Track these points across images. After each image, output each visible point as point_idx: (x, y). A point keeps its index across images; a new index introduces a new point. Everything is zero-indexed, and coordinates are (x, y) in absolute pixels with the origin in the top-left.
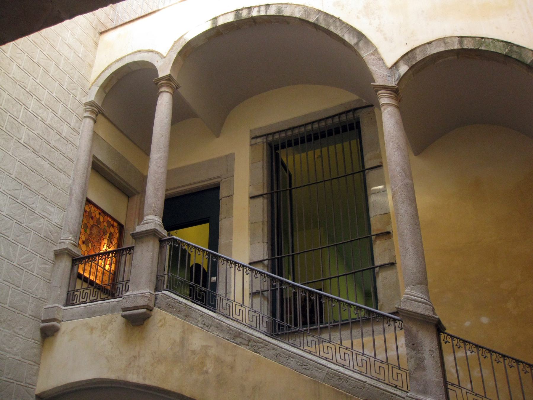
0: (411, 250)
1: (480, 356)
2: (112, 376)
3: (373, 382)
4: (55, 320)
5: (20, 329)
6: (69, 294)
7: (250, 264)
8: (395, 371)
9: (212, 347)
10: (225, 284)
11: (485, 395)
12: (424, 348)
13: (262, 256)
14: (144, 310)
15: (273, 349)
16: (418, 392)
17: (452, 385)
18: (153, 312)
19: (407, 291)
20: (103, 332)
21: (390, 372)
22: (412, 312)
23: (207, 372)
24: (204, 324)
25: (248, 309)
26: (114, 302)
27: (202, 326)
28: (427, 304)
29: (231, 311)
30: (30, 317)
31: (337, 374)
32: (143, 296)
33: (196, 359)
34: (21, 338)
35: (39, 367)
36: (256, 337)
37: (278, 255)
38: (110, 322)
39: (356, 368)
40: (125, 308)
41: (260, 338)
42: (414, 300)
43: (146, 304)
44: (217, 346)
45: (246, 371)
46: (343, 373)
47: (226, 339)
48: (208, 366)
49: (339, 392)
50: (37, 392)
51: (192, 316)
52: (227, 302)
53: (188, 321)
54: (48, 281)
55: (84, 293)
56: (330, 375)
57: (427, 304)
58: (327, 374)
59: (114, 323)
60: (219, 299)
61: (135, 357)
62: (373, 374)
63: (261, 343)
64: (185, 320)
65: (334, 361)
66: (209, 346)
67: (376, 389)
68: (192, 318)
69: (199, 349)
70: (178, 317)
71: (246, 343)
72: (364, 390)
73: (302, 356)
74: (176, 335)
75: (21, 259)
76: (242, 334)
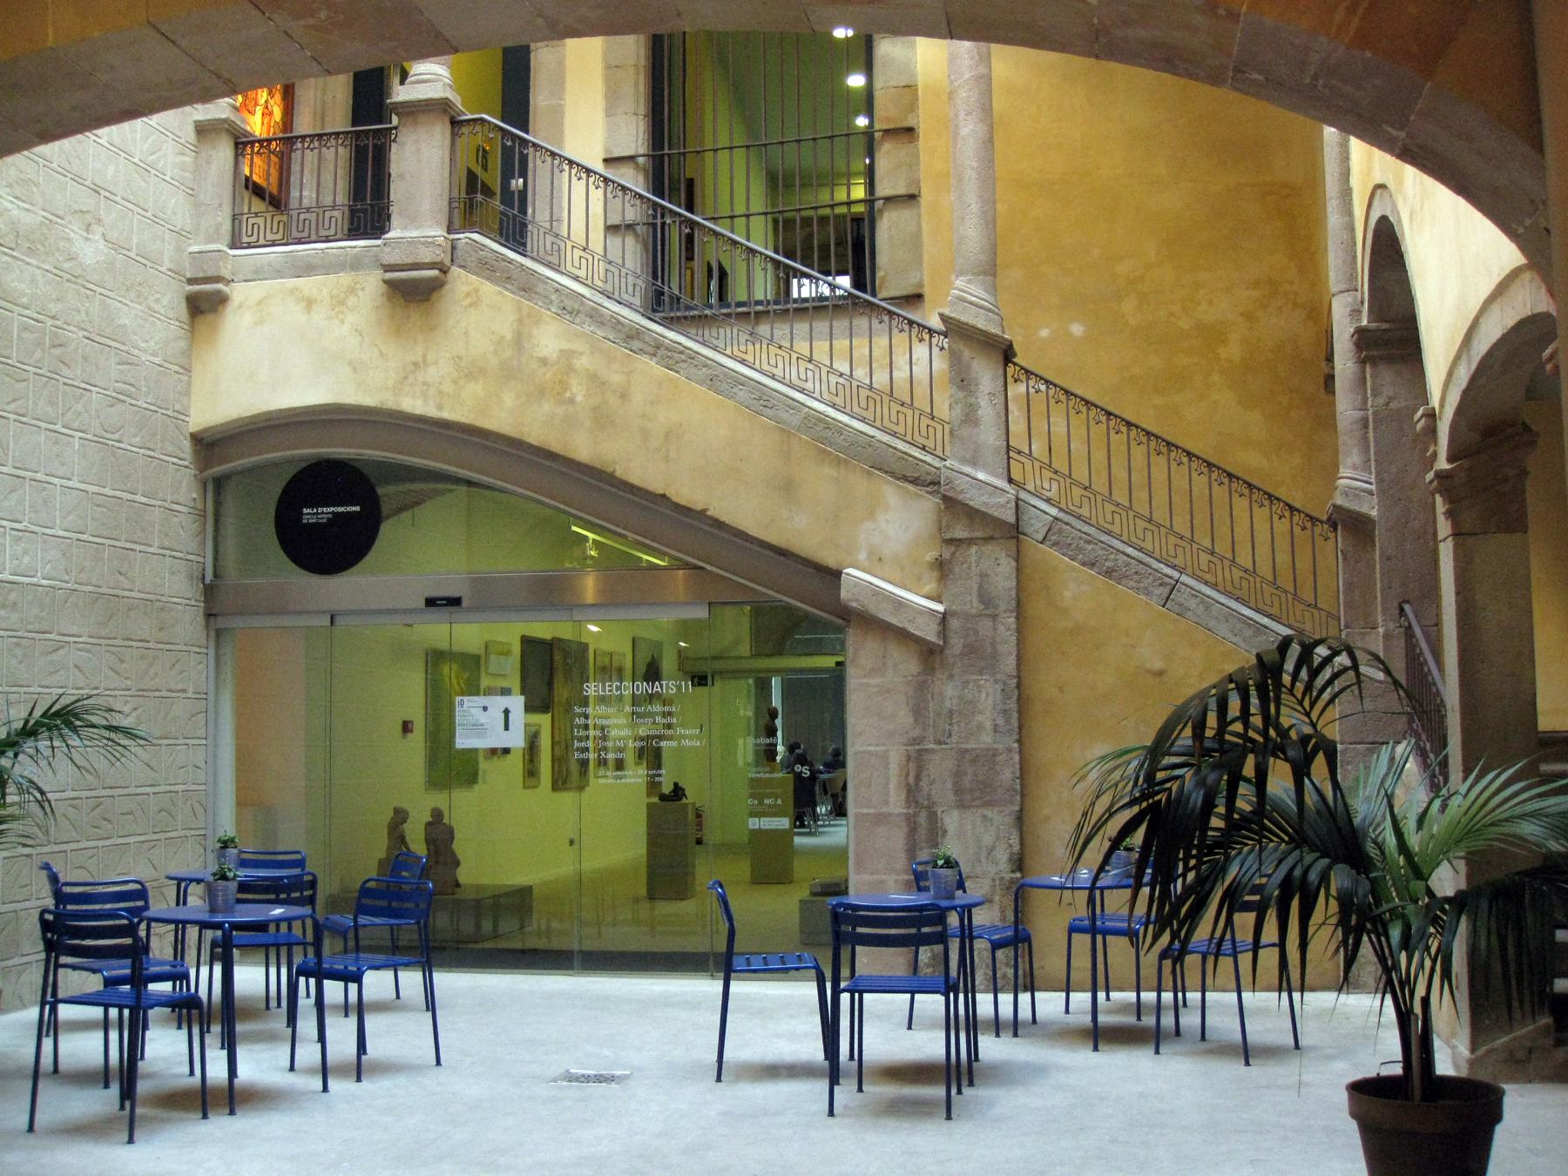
0: (975, 207)
1: (1071, 410)
2: (368, 401)
3: (886, 438)
4: (218, 279)
5: (157, 301)
6: (237, 222)
7: (606, 161)
8: (925, 421)
9: (581, 354)
10: (548, 199)
11: (1131, 505)
12: (981, 387)
13: (633, 145)
14: (434, 273)
15: (704, 366)
16: (964, 461)
17: (1019, 452)
18: (450, 276)
19: (959, 283)
20: (337, 309)
21: (916, 422)
22: (967, 324)
23: (572, 401)
24: (564, 308)
25: (596, 257)
26: (355, 247)
27: (560, 312)
28: (992, 312)
29: (563, 257)
30: (169, 273)
31: (821, 419)
32: (429, 243)
33: (548, 376)
34: (159, 319)
35: (190, 377)
36: (671, 340)
37: (669, 149)
38: (352, 291)
39: (825, 395)
40: (389, 265)
41: (680, 344)
42: (971, 303)
43: (438, 259)
44: (592, 353)
45: (652, 403)
46: (834, 419)
47: (609, 340)
48: (574, 390)
49: (825, 450)
50: (193, 428)
51: (537, 290)
52: (553, 239)
53: (529, 300)
54: (190, 192)
55: (307, 230)
56: (809, 421)
57: (992, 312)
58: (805, 418)
59: (360, 293)
60: (535, 232)
61: (416, 364)
62: (856, 409)
63: (681, 353)
64: (522, 297)
65: (817, 395)
66: (574, 352)
67: (891, 450)
68: (536, 293)
69: (555, 355)
70: (507, 289)
71: (651, 350)
72: (870, 450)
73: (759, 383)
74: (505, 325)
75: (146, 146)
76: (644, 333)
